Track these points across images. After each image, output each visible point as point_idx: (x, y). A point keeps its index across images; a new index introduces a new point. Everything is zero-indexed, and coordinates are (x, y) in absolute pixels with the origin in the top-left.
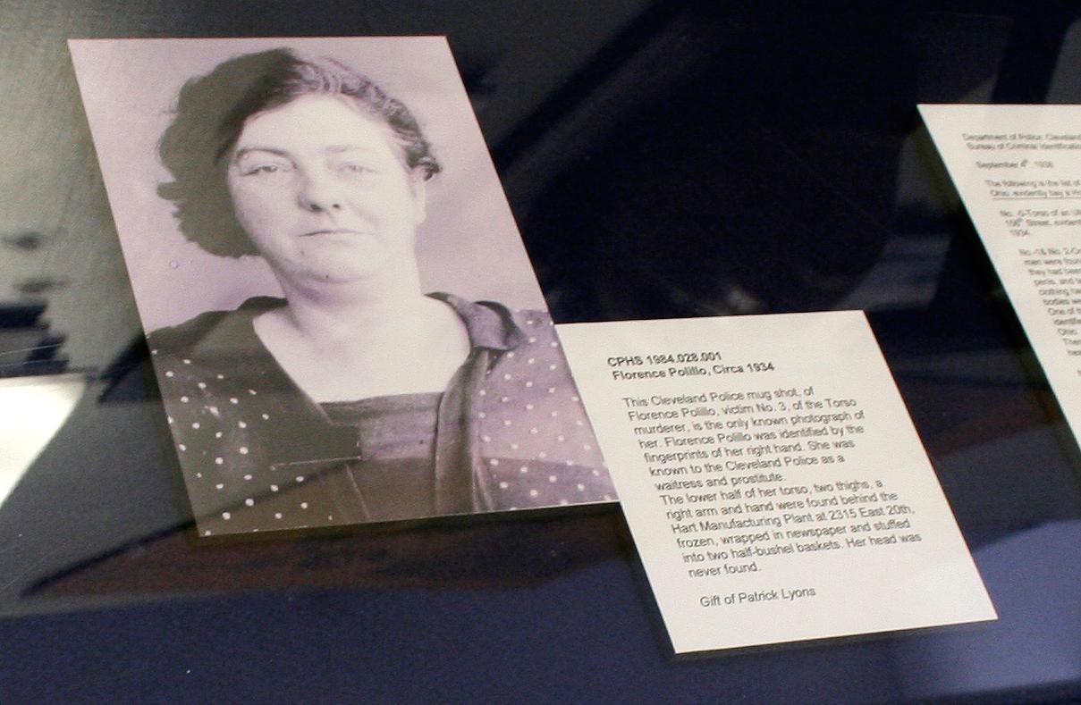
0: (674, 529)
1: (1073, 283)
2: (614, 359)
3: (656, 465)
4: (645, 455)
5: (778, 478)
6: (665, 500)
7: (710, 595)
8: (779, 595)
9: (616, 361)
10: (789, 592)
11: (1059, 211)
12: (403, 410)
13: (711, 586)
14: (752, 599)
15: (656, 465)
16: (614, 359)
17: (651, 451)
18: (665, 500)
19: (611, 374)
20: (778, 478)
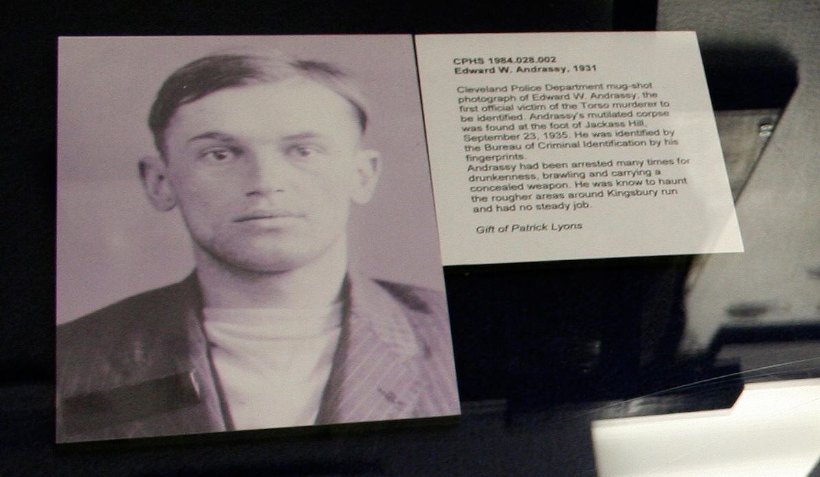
0: (576, 185)
1: (527, 129)
2: (459, 60)
3: (475, 164)
4: (467, 157)
5: (521, 157)
6: (584, 106)
7: (486, 225)
8: (549, 227)
9: (461, 61)
10: (559, 226)
11: (561, 71)
12: (196, 98)
13: (485, 219)
14: (523, 229)
15: (475, 164)
16: (459, 60)
17: (473, 153)
18: (584, 106)
19: (457, 99)
20: (521, 157)
